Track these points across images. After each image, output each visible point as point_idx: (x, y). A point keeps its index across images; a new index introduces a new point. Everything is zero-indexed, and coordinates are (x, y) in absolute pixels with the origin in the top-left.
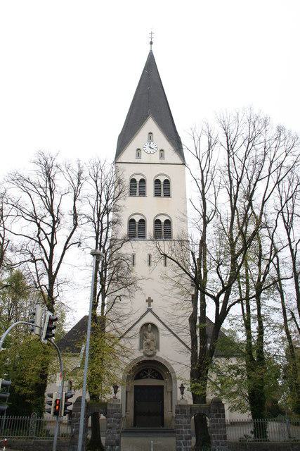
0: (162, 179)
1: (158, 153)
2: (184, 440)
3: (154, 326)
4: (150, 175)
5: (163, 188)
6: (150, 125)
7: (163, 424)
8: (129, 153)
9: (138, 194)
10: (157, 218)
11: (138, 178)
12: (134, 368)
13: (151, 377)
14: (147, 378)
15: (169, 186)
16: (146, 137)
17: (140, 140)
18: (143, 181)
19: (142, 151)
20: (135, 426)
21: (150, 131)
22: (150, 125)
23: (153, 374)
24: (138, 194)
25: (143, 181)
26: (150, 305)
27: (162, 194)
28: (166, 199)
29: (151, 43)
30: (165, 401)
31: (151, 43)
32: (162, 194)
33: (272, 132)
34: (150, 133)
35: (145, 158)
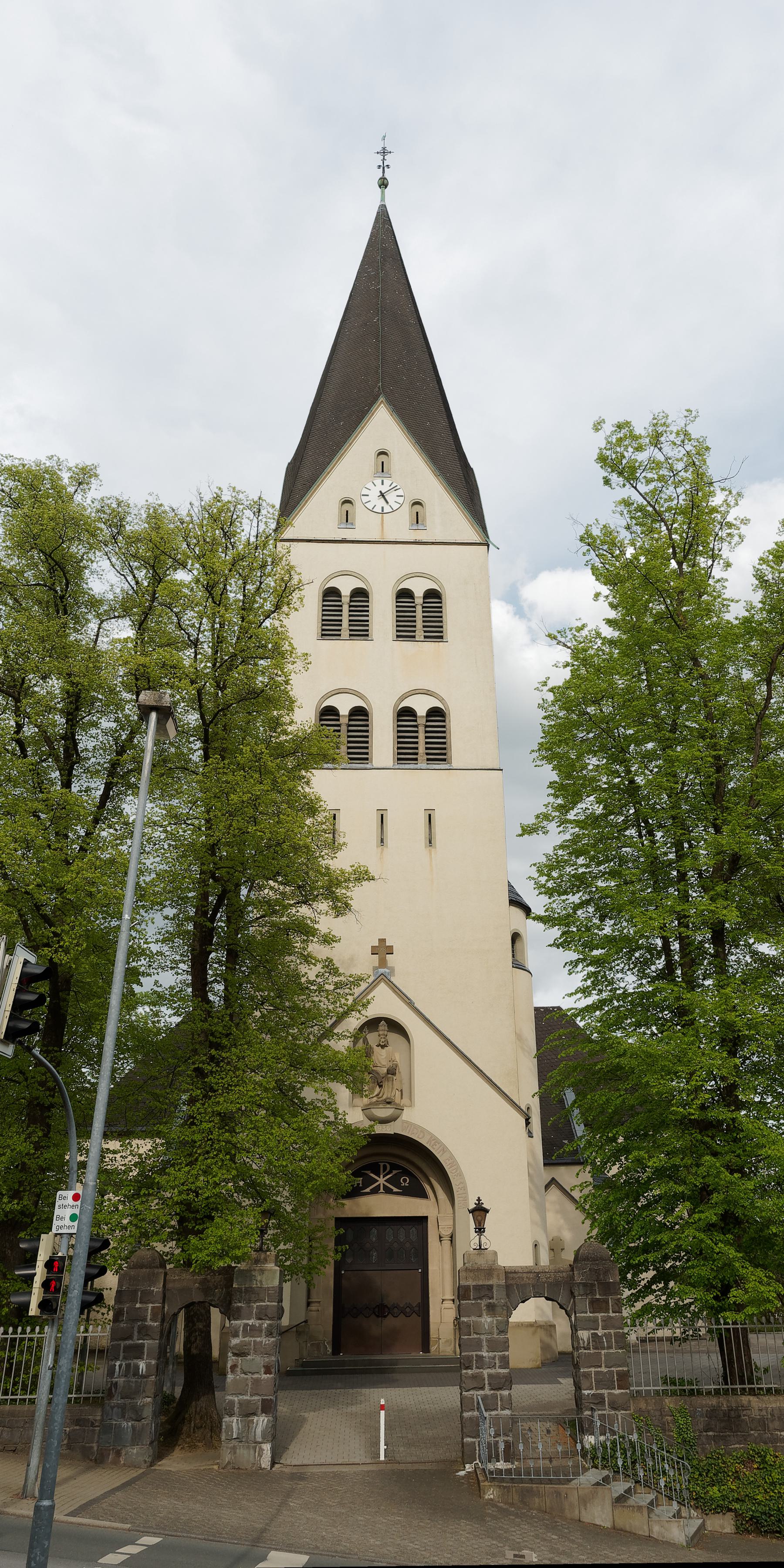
0: (419, 588)
1: (406, 514)
2: (487, 1391)
3: (395, 1027)
4: (382, 575)
5: (422, 615)
6: (382, 427)
7: (425, 1345)
8: (318, 512)
9: (345, 633)
10: (404, 704)
11: (346, 587)
12: (293, 1437)
13: (388, 1191)
14: (375, 1191)
15: (440, 609)
16: (370, 462)
17: (349, 470)
18: (360, 594)
19: (358, 505)
20: (336, 1351)
21: (418, 497)
22: (382, 427)
23: (394, 1181)
24: (345, 633)
25: (360, 594)
26: (383, 963)
27: (420, 634)
28: (430, 647)
29: (383, 184)
30: (433, 1267)
31: (383, 184)
32: (420, 634)
33: (154, 534)
34: (383, 453)
35: (365, 525)
